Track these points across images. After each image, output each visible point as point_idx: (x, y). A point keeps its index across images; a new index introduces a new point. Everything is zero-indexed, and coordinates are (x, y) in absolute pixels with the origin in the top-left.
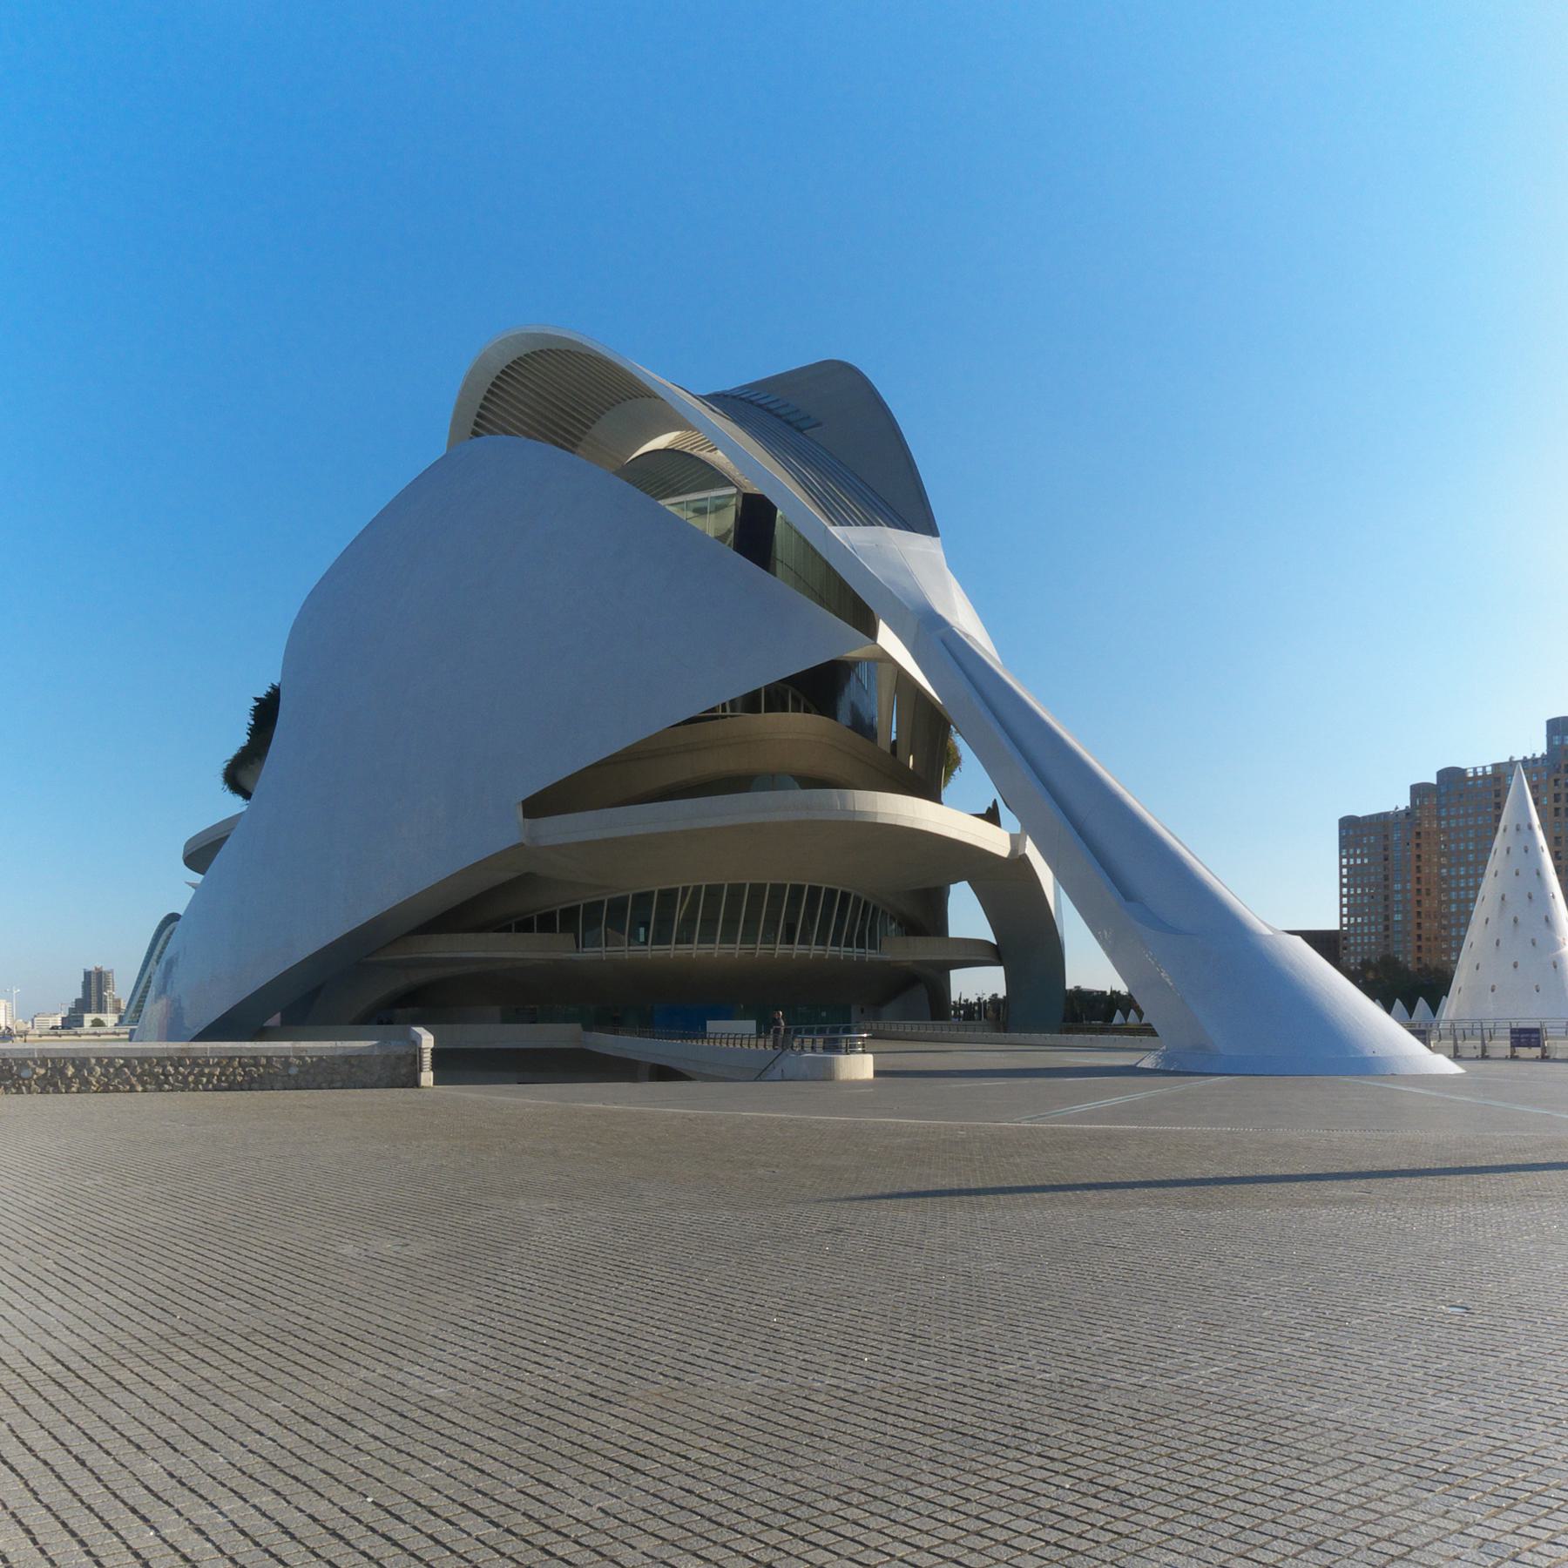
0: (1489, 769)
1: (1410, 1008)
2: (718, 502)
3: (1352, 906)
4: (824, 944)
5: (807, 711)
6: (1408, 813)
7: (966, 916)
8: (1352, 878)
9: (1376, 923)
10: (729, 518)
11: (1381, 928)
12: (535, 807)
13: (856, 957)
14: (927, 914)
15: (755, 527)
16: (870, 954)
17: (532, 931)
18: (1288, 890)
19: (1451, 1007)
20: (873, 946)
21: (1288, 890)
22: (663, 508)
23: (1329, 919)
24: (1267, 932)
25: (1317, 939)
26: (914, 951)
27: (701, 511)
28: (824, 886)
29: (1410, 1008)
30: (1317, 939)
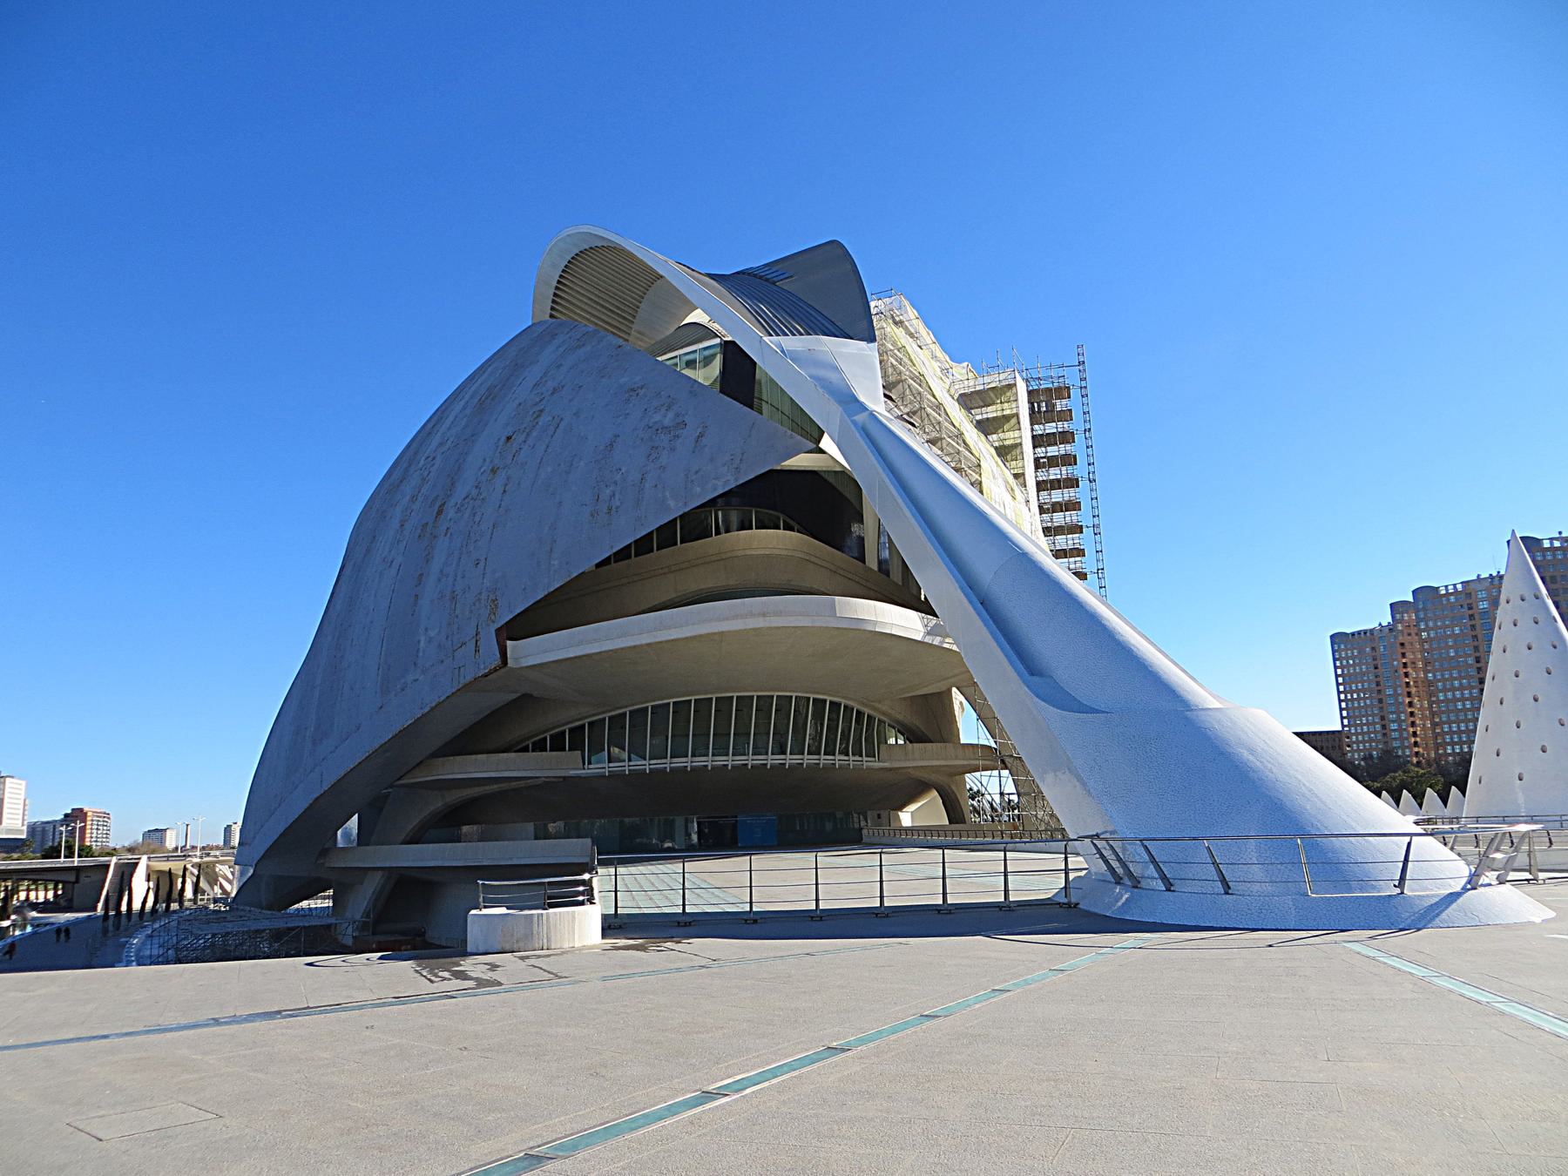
0: (1459, 587)
1: (1419, 798)
2: (707, 353)
3: (1349, 710)
5: (788, 527)
6: (1391, 628)
8: (1346, 682)
9: (1374, 723)
10: (716, 366)
11: (1378, 727)
13: (795, 779)
14: (930, 721)
15: (739, 374)
16: (868, 763)
18: (1272, 697)
19: (1470, 802)
20: (870, 754)
21: (1272, 697)
22: (671, 370)
23: (1331, 721)
24: (1214, 704)
25: (1311, 739)
26: (924, 758)
27: (691, 364)
28: (735, 695)
29: (1419, 798)
30: (1311, 739)
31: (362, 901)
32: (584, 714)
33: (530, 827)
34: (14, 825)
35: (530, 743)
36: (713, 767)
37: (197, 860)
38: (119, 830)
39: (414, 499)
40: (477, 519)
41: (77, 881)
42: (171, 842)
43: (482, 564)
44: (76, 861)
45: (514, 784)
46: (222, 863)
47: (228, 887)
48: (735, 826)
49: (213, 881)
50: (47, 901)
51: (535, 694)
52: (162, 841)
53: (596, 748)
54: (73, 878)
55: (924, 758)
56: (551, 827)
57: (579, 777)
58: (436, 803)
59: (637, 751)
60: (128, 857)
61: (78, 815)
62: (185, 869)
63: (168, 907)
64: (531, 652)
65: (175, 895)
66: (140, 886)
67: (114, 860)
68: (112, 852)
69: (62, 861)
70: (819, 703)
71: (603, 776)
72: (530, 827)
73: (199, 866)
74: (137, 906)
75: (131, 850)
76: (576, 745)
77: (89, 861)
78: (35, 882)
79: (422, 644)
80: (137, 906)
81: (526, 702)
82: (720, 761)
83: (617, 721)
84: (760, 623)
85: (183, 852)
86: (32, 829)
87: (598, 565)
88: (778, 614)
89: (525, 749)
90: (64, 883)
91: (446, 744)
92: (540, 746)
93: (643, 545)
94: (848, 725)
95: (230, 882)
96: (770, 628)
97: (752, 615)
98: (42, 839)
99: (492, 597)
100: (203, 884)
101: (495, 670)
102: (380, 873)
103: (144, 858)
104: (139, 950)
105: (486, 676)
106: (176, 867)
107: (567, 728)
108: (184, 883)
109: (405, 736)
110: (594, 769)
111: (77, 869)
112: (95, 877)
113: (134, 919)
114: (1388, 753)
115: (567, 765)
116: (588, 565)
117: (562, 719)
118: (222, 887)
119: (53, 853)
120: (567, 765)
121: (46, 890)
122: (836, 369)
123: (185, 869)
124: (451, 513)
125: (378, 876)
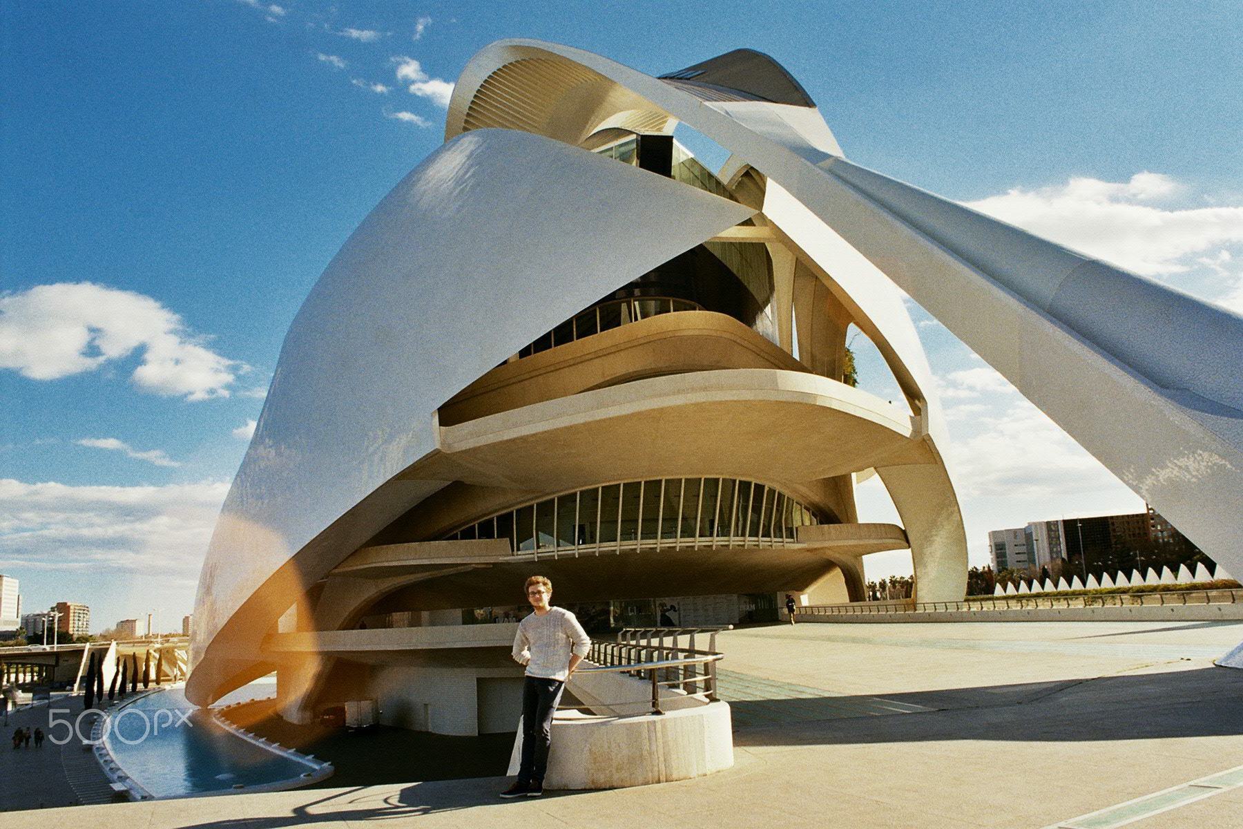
4: (743, 535)
7: (872, 500)
12: (451, 413)
14: (833, 507)
17: (491, 536)
32: (512, 501)
33: (458, 613)
34: (8, 620)
35: (458, 531)
36: (642, 551)
37: (158, 646)
38: (94, 621)
41: (57, 664)
42: (140, 630)
44: (56, 647)
45: (445, 572)
46: (180, 648)
47: (184, 668)
49: (173, 662)
50: (24, 683)
51: (468, 481)
52: (133, 629)
53: (524, 536)
55: (831, 540)
56: (479, 612)
57: (508, 564)
58: (370, 591)
59: (565, 536)
60: (101, 643)
62: (148, 653)
63: (134, 687)
65: (141, 676)
66: (109, 669)
67: (88, 646)
68: (84, 639)
70: (745, 486)
72: (458, 613)
73: (160, 651)
74: (107, 686)
75: (104, 637)
76: (505, 532)
77: (67, 647)
78: (24, 665)
80: (107, 686)
81: (457, 491)
82: (649, 543)
83: (545, 508)
84: (700, 397)
85: (147, 640)
86: (26, 621)
87: (524, 353)
88: (720, 388)
89: (455, 538)
90: (40, 666)
91: (381, 533)
92: (468, 534)
94: (757, 504)
95: (185, 663)
96: (714, 403)
97: (693, 389)
98: (33, 630)
100: (165, 667)
103: (114, 643)
106: (140, 651)
108: (147, 666)
111: (57, 655)
112: (72, 661)
113: (105, 698)
114: (531, 609)
117: (492, 507)
118: (180, 669)
119: (37, 639)
121: (25, 673)
122: (786, 126)
123: (148, 653)
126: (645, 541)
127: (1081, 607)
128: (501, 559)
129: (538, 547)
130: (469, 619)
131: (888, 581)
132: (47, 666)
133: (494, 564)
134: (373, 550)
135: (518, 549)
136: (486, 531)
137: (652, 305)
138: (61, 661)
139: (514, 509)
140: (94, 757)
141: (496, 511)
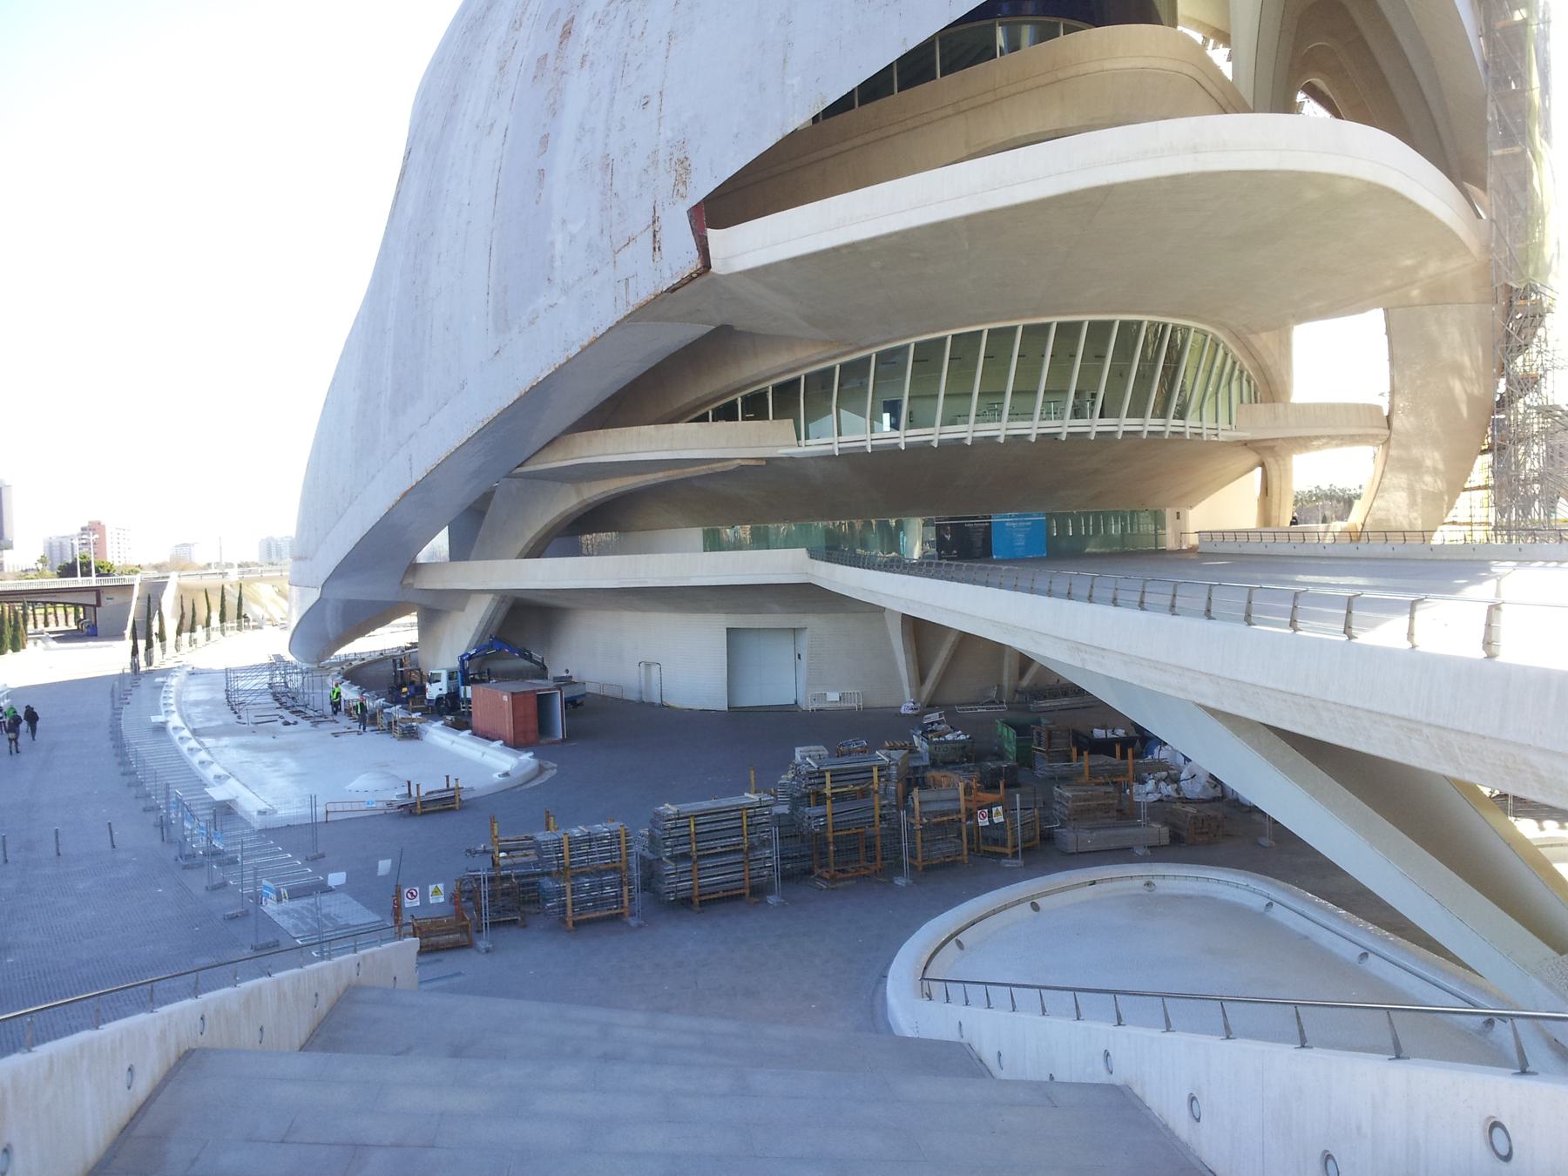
4: (1164, 415)
17: (764, 416)
26: (1255, 423)
31: (460, 636)
35: (710, 410)
39: (516, 25)
40: (637, 29)
41: (99, 604)
43: (655, 102)
45: (718, 467)
48: (988, 530)
51: (740, 325)
53: (817, 410)
54: (92, 600)
58: (568, 501)
61: (94, 527)
64: (748, 246)
69: (79, 581)
71: (830, 457)
79: (558, 247)
81: (720, 342)
87: (815, 119)
92: (727, 413)
93: (874, 89)
99: (678, 155)
101: (691, 279)
102: (489, 597)
104: (179, 694)
105: (673, 290)
107: (769, 385)
109: (537, 395)
110: (814, 446)
111: (97, 591)
112: (118, 598)
115: (770, 440)
116: (799, 118)
117: (763, 369)
119: (68, 571)
120: (770, 440)
124: (585, 29)
125: (489, 597)
126: (981, 426)
127: (331, 876)
128: (782, 452)
129: (840, 434)
130: (713, 543)
131: (21, 714)
132: (84, 606)
133: (768, 460)
134: (581, 438)
135: (807, 438)
136: (755, 407)
137: (1026, 32)
138: (104, 601)
139: (802, 373)
140: (170, 741)
141: (771, 377)
